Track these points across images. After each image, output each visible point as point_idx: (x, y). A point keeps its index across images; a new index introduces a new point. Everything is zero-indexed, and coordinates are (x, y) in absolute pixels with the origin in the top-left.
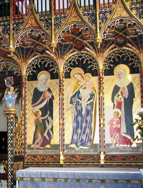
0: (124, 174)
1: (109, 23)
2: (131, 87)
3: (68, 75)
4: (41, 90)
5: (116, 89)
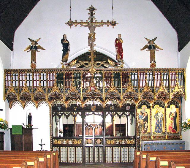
1: (174, 93)
2: (176, 113)
3: (153, 107)
5: (171, 113)
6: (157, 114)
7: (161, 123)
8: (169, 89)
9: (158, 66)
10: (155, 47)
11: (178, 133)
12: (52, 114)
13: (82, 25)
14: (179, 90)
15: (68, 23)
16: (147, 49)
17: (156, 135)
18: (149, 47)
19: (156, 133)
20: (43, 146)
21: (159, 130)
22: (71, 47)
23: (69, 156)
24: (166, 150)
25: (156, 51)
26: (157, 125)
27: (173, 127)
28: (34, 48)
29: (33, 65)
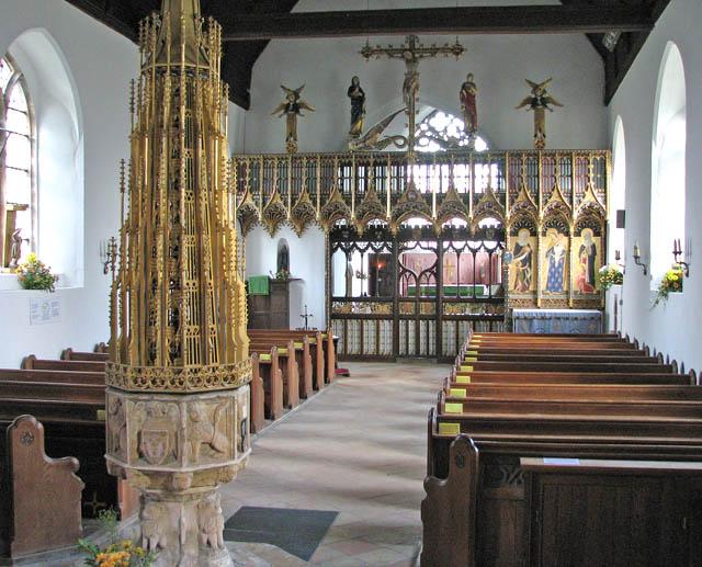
0: (525, 413)
1: (582, 205)
2: (593, 247)
3: (544, 234)
4: (521, 245)
5: (583, 248)
8: (571, 197)
9: (550, 145)
10: (545, 102)
11: (599, 292)
12: (331, 246)
13: (391, 56)
14: (559, 200)
15: (363, 53)
16: (529, 106)
17: (548, 297)
18: (533, 103)
20: (309, 319)
22: (367, 105)
23: (365, 340)
24: (552, 331)
25: (546, 111)
26: (552, 274)
27: (587, 280)
28: (293, 108)
29: (291, 148)
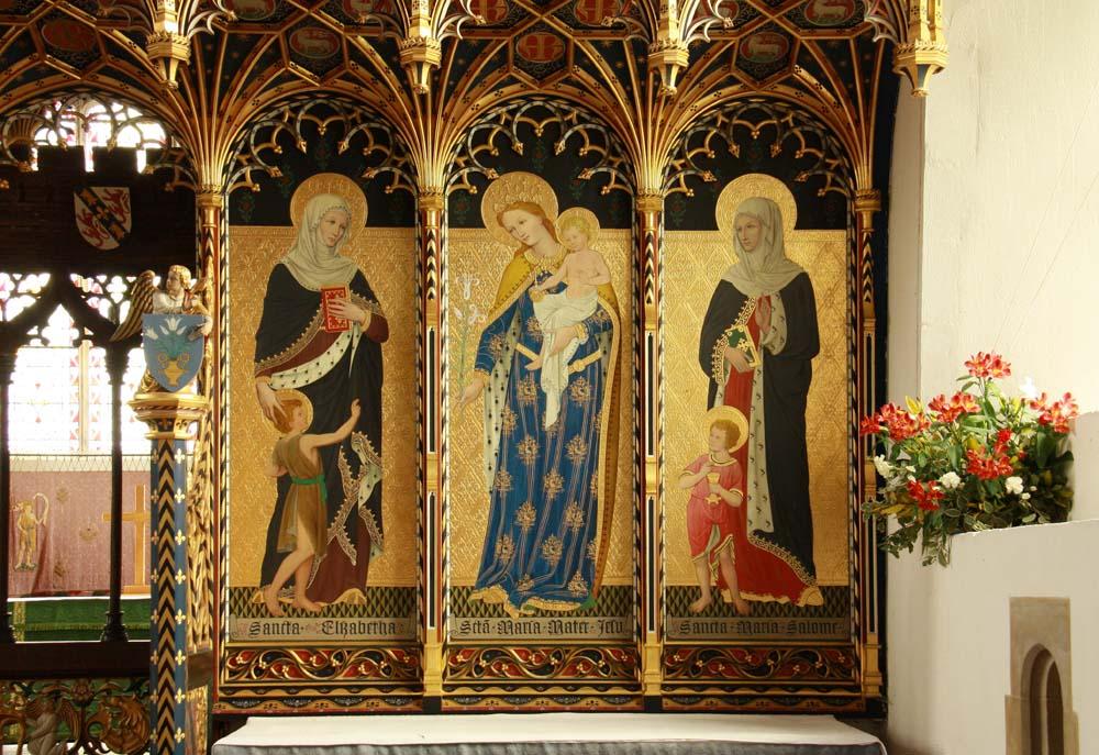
5: (726, 303)
6: (523, 310)
7: (578, 450)
11: (836, 598)
19: (496, 594)
21: (552, 551)
27: (759, 516)
